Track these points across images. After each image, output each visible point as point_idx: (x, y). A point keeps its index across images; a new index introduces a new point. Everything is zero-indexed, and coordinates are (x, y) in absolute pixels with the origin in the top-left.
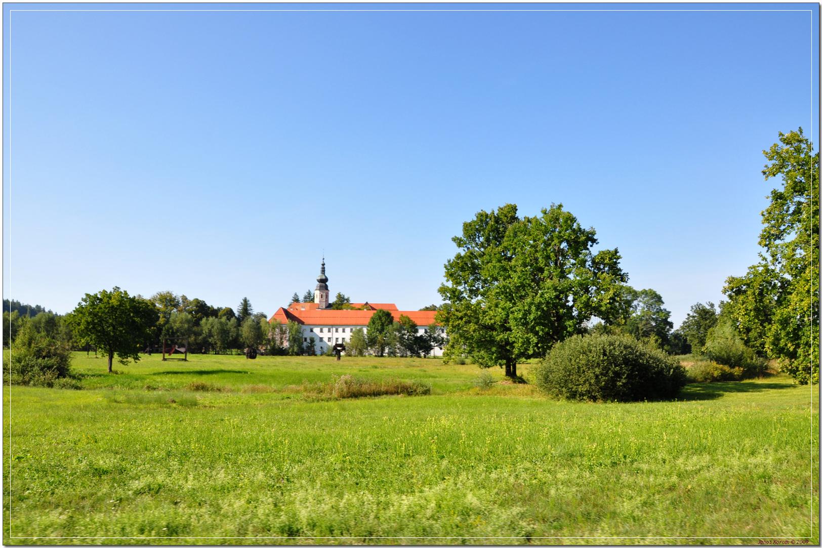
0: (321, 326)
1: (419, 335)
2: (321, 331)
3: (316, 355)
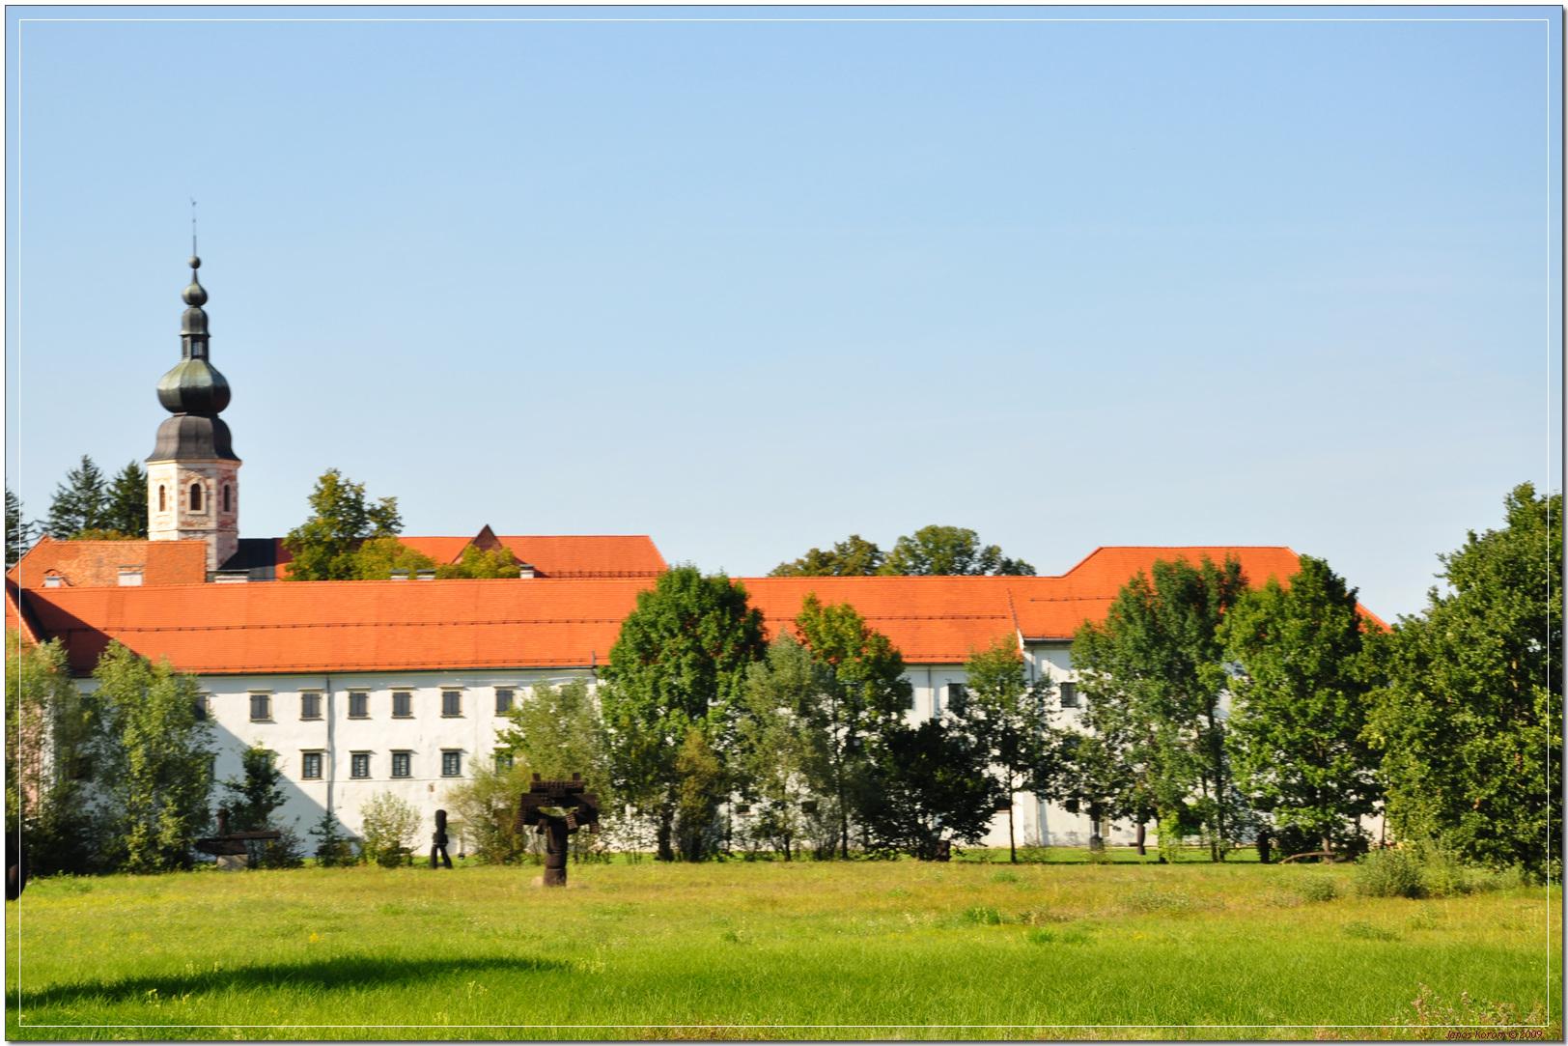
0: (260, 682)
1: (914, 719)
2: (260, 712)
3: (295, 863)
